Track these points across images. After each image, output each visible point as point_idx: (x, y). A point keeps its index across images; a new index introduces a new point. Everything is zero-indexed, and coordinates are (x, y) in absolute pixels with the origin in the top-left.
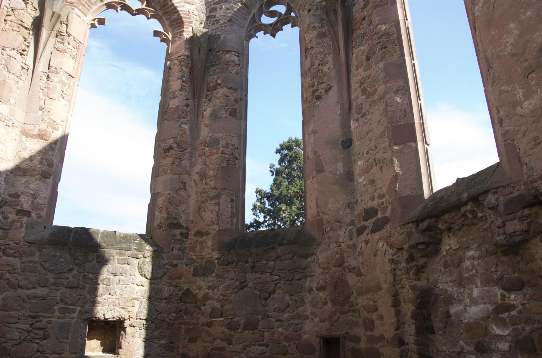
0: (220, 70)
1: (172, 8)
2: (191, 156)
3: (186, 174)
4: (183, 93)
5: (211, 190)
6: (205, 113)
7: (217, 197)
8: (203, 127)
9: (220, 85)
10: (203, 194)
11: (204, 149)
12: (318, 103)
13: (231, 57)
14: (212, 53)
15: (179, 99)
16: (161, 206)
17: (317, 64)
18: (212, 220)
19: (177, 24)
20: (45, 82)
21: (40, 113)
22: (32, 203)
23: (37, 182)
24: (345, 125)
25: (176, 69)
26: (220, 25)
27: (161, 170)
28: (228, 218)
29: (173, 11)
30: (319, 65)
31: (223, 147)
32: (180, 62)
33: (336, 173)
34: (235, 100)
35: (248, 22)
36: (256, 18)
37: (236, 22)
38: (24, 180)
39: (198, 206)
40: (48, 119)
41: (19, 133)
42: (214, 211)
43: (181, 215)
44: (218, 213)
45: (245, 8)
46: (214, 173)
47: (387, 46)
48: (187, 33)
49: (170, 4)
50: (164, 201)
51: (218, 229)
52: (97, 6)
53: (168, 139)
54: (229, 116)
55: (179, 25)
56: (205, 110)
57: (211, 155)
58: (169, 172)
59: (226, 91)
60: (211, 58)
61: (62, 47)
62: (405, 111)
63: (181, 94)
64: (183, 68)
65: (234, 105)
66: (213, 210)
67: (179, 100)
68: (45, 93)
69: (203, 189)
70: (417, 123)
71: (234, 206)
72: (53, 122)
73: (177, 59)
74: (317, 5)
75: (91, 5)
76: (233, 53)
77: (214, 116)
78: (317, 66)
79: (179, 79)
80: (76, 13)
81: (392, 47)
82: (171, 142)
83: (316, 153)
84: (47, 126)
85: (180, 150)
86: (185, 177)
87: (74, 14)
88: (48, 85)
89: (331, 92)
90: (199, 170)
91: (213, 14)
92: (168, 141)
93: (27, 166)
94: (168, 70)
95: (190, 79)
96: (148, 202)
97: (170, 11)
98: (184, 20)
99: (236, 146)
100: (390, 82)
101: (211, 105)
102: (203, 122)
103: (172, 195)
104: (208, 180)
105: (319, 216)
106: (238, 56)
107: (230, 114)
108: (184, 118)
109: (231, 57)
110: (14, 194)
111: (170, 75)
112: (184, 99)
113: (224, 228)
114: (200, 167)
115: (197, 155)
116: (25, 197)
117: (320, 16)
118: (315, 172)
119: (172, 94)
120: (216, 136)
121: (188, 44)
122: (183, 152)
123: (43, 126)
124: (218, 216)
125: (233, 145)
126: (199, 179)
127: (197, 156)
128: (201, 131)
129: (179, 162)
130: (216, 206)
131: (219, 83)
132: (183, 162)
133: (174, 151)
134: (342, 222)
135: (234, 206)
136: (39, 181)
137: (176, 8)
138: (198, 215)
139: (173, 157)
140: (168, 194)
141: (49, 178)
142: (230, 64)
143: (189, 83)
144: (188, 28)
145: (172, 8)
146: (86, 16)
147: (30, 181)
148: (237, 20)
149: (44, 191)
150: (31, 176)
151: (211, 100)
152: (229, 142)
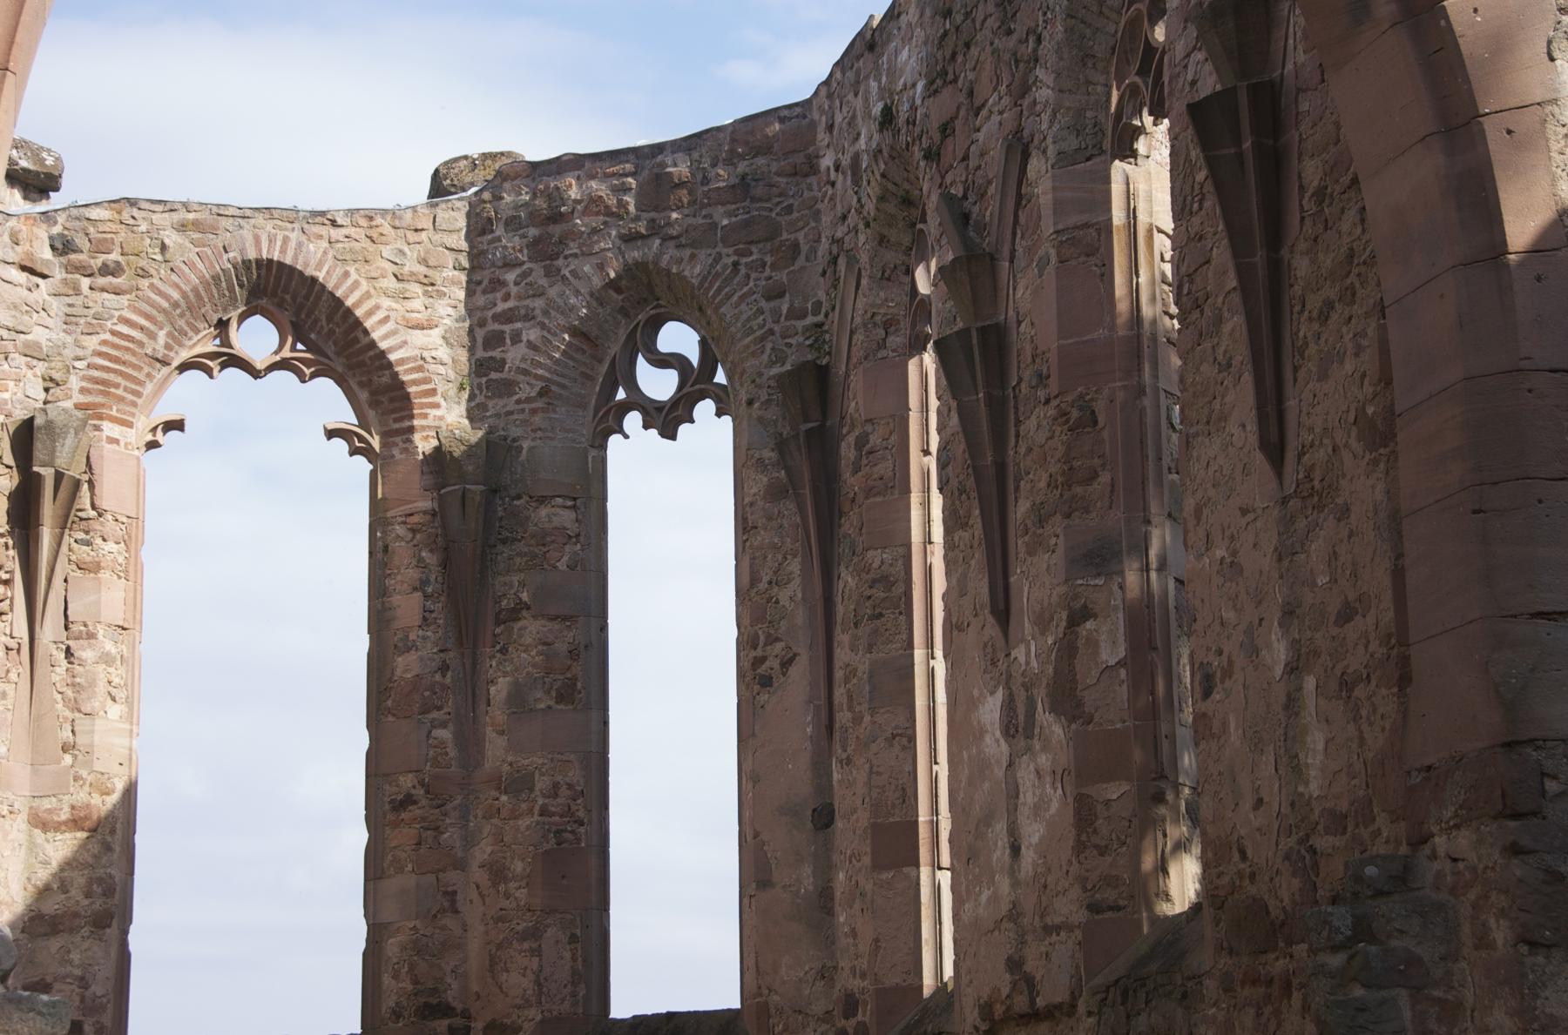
0: (525, 559)
1: (371, 353)
2: (463, 817)
3: (456, 869)
4: (429, 634)
5: (520, 913)
6: (493, 689)
7: (534, 933)
8: (490, 733)
9: (528, 608)
10: (500, 924)
11: (497, 799)
12: (764, 697)
13: (554, 519)
14: (501, 498)
15: (419, 653)
16: (395, 960)
17: (765, 579)
18: (524, 995)
19: (392, 400)
20: (65, 668)
21: (68, 759)
22: (83, 1000)
23: (86, 945)
24: (821, 768)
25: (402, 553)
26: (518, 402)
27: (388, 862)
28: (565, 986)
29: (377, 364)
30: (770, 583)
31: (544, 796)
32: (413, 531)
33: (798, 891)
34: (570, 652)
35: (598, 388)
36: (618, 375)
37: (560, 394)
38: (55, 944)
39: (490, 955)
40: (89, 774)
41: (24, 826)
42: (529, 971)
43: (449, 981)
44: (538, 976)
45: (584, 347)
46: (524, 869)
47: (884, 612)
48: (425, 434)
49: (365, 341)
50: (404, 948)
51: (539, 1017)
52: (155, 381)
53: (401, 773)
54: (557, 703)
55: (397, 405)
56: (492, 682)
57: (516, 818)
58: (410, 867)
59: (546, 629)
60: (500, 514)
61: (88, 554)
62: (904, 789)
63: (425, 638)
64: (424, 554)
65: (569, 668)
66: (526, 968)
67: (421, 659)
68: (70, 700)
69: (501, 909)
70: (925, 822)
71: (580, 952)
72: (99, 776)
73: (404, 523)
74: (769, 387)
75: (138, 388)
76: (559, 500)
77: (517, 698)
78: (766, 586)
79: (415, 589)
80: (108, 437)
81: (892, 616)
82: (407, 781)
83: (756, 835)
84: (90, 794)
85: (434, 803)
86: (453, 876)
87: (104, 443)
88: (74, 677)
89: (795, 671)
90: (486, 857)
91: (496, 354)
92: (401, 778)
93: (57, 907)
94: (380, 556)
95: (445, 586)
96: (361, 945)
97: (369, 362)
98: (412, 389)
99: (579, 788)
100: (882, 710)
101: (508, 669)
102: (491, 717)
103: (421, 932)
104: (512, 885)
105: (761, 995)
106: (574, 507)
107: (560, 698)
108: (439, 708)
109: (554, 519)
110: (37, 983)
111: (389, 572)
112: (435, 651)
113: (555, 1013)
114: (489, 850)
115: (480, 813)
116: (63, 987)
117: (776, 427)
118: (754, 885)
119: (400, 635)
120: (526, 762)
121: (431, 472)
122: (443, 808)
123: (81, 795)
124: (540, 985)
125: (570, 786)
126: (490, 883)
127: (480, 815)
128: (487, 744)
129: (435, 837)
130: (533, 959)
131: (526, 603)
132: (445, 836)
133: (419, 808)
134: (807, 1014)
135: (580, 952)
136: (89, 941)
137: (383, 354)
138: (490, 980)
139: (418, 826)
140: (411, 929)
141: (109, 926)
142: (553, 542)
143: (443, 599)
144: (425, 416)
145: (371, 353)
146: (130, 425)
147: (70, 946)
148: (563, 387)
149: (102, 961)
150: (71, 931)
151: (507, 651)
152: (559, 778)
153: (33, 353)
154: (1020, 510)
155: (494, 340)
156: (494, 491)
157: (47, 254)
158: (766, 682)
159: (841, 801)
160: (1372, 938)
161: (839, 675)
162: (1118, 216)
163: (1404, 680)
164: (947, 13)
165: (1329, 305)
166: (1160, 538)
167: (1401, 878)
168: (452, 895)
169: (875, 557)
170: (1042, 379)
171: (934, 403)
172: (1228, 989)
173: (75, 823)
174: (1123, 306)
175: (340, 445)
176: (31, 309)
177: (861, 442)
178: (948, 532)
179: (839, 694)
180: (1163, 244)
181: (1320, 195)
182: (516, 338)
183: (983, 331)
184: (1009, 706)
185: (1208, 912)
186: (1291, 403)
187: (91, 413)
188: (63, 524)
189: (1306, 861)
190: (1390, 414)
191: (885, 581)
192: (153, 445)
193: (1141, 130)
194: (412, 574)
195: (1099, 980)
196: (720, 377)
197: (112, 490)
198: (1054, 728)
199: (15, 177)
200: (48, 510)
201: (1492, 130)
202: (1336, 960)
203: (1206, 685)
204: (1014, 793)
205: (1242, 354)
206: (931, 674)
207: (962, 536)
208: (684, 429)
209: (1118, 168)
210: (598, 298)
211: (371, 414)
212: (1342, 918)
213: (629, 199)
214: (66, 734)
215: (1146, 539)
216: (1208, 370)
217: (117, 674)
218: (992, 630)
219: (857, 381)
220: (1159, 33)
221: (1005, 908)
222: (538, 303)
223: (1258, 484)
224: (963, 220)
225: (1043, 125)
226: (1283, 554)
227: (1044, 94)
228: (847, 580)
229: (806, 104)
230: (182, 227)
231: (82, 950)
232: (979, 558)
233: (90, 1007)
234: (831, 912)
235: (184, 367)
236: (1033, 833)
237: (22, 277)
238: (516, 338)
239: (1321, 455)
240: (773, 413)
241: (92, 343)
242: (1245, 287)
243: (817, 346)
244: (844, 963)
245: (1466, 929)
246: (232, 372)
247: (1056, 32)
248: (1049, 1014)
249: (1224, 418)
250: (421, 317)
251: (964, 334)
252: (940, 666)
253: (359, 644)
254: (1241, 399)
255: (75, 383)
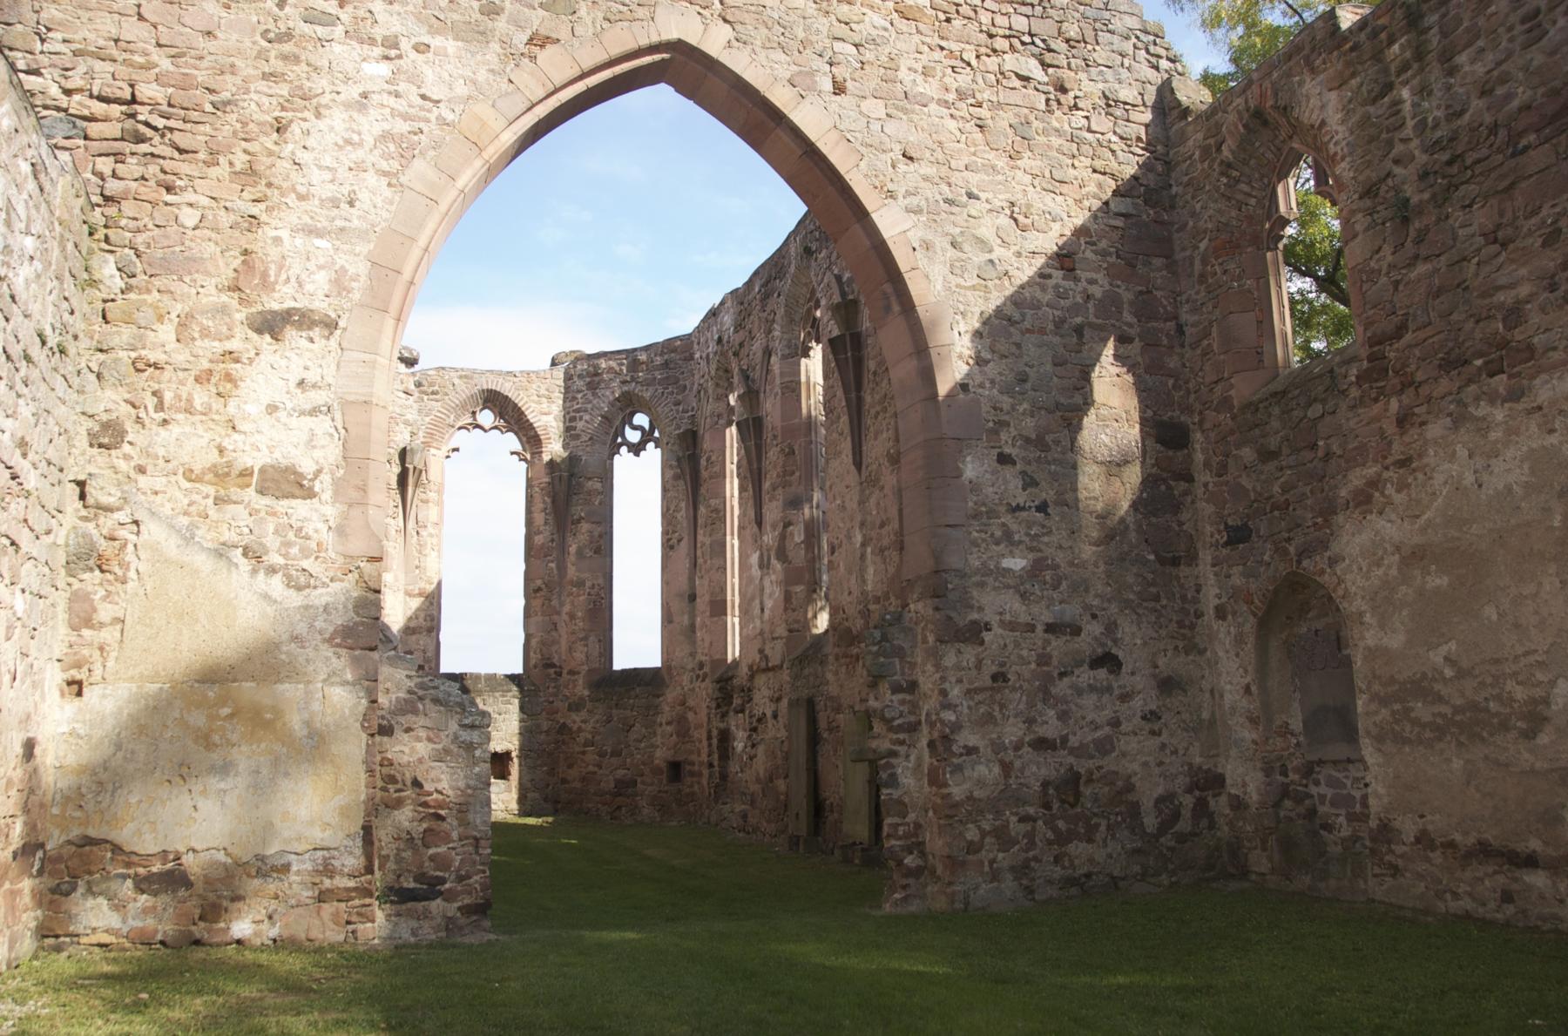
7: (586, 638)
8: (569, 565)
24: (692, 580)
25: (538, 498)
38: (414, 638)
77: (580, 553)
82: (539, 582)
86: (555, 617)
153: (407, 423)
154: (767, 485)
155: (573, 419)
156: (572, 475)
157: (413, 387)
158: (672, 547)
159: (698, 593)
160: (887, 641)
161: (699, 545)
162: (803, 379)
163: (902, 549)
164: (742, 303)
165: (878, 413)
166: (817, 496)
167: (898, 618)
168: (555, 624)
169: (713, 502)
170: (775, 437)
171: (735, 445)
172: (837, 659)
173: (420, 595)
174: (804, 411)
175: (515, 457)
176: (407, 407)
177: (708, 460)
178: (740, 493)
179: (699, 553)
180: (820, 390)
181: (875, 373)
182: (581, 418)
183: (754, 419)
184: (761, 557)
185: (831, 633)
186: (864, 448)
187: (427, 445)
188: (416, 486)
189: (865, 614)
190: (899, 453)
191: (716, 511)
192: (448, 457)
193: (811, 348)
194: (542, 506)
195: (791, 657)
196: (656, 434)
197: (434, 473)
198: (777, 565)
199: (402, 359)
200: (411, 480)
201: (933, 352)
202: (875, 648)
203: (833, 550)
204: (762, 590)
205: (847, 430)
206: (733, 546)
207: (745, 494)
208: (642, 453)
209: (803, 361)
210: (611, 404)
211: (527, 446)
212: (877, 634)
213: (624, 368)
214: (417, 562)
215: (812, 496)
216: (835, 435)
217: (435, 541)
218: (755, 529)
219: (707, 436)
220: (818, 314)
221: (758, 631)
222: (589, 406)
223: (852, 478)
224: (747, 378)
225: (777, 345)
226: (861, 503)
227: (777, 333)
228: (702, 510)
229: (690, 335)
230: (461, 377)
231: (423, 640)
232: (751, 502)
233: (427, 660)
234: (694, 632)
235: (460, 428)
236: (769, 604)
237: (404, 396)
238: (581, 418)
239: (874, 467)
240: (676, 448)
241: (427, 419)
242: (848, 405)
243: (693, 423)
244: (699, 651)
245: (920, 637)
246: (477, 430)
247: (781, 312)
248: (773, 669)
249: (840, 453)
250: (546, 410)
251: (747, 420)
252: (736, 542)
253: (521, 531)
254: (846, 446)
255: (421, 434)
